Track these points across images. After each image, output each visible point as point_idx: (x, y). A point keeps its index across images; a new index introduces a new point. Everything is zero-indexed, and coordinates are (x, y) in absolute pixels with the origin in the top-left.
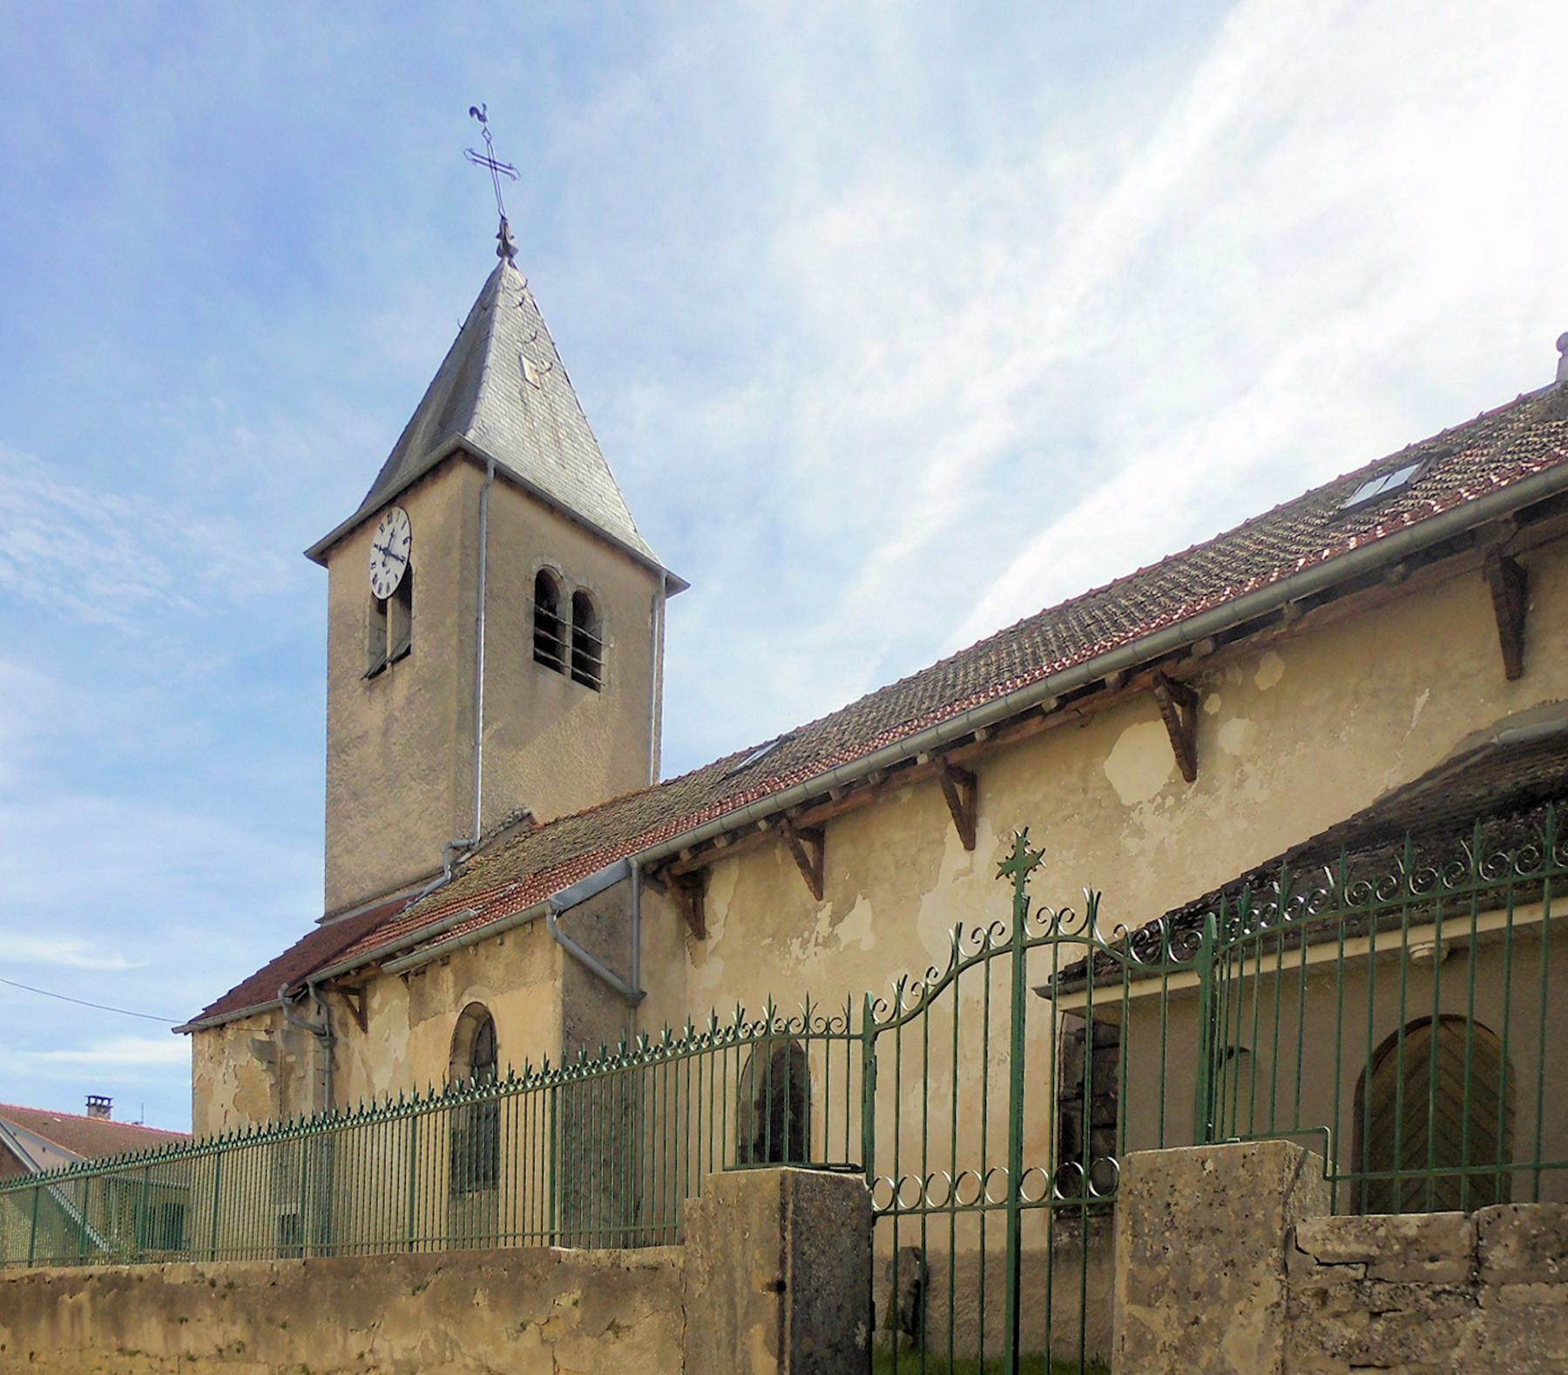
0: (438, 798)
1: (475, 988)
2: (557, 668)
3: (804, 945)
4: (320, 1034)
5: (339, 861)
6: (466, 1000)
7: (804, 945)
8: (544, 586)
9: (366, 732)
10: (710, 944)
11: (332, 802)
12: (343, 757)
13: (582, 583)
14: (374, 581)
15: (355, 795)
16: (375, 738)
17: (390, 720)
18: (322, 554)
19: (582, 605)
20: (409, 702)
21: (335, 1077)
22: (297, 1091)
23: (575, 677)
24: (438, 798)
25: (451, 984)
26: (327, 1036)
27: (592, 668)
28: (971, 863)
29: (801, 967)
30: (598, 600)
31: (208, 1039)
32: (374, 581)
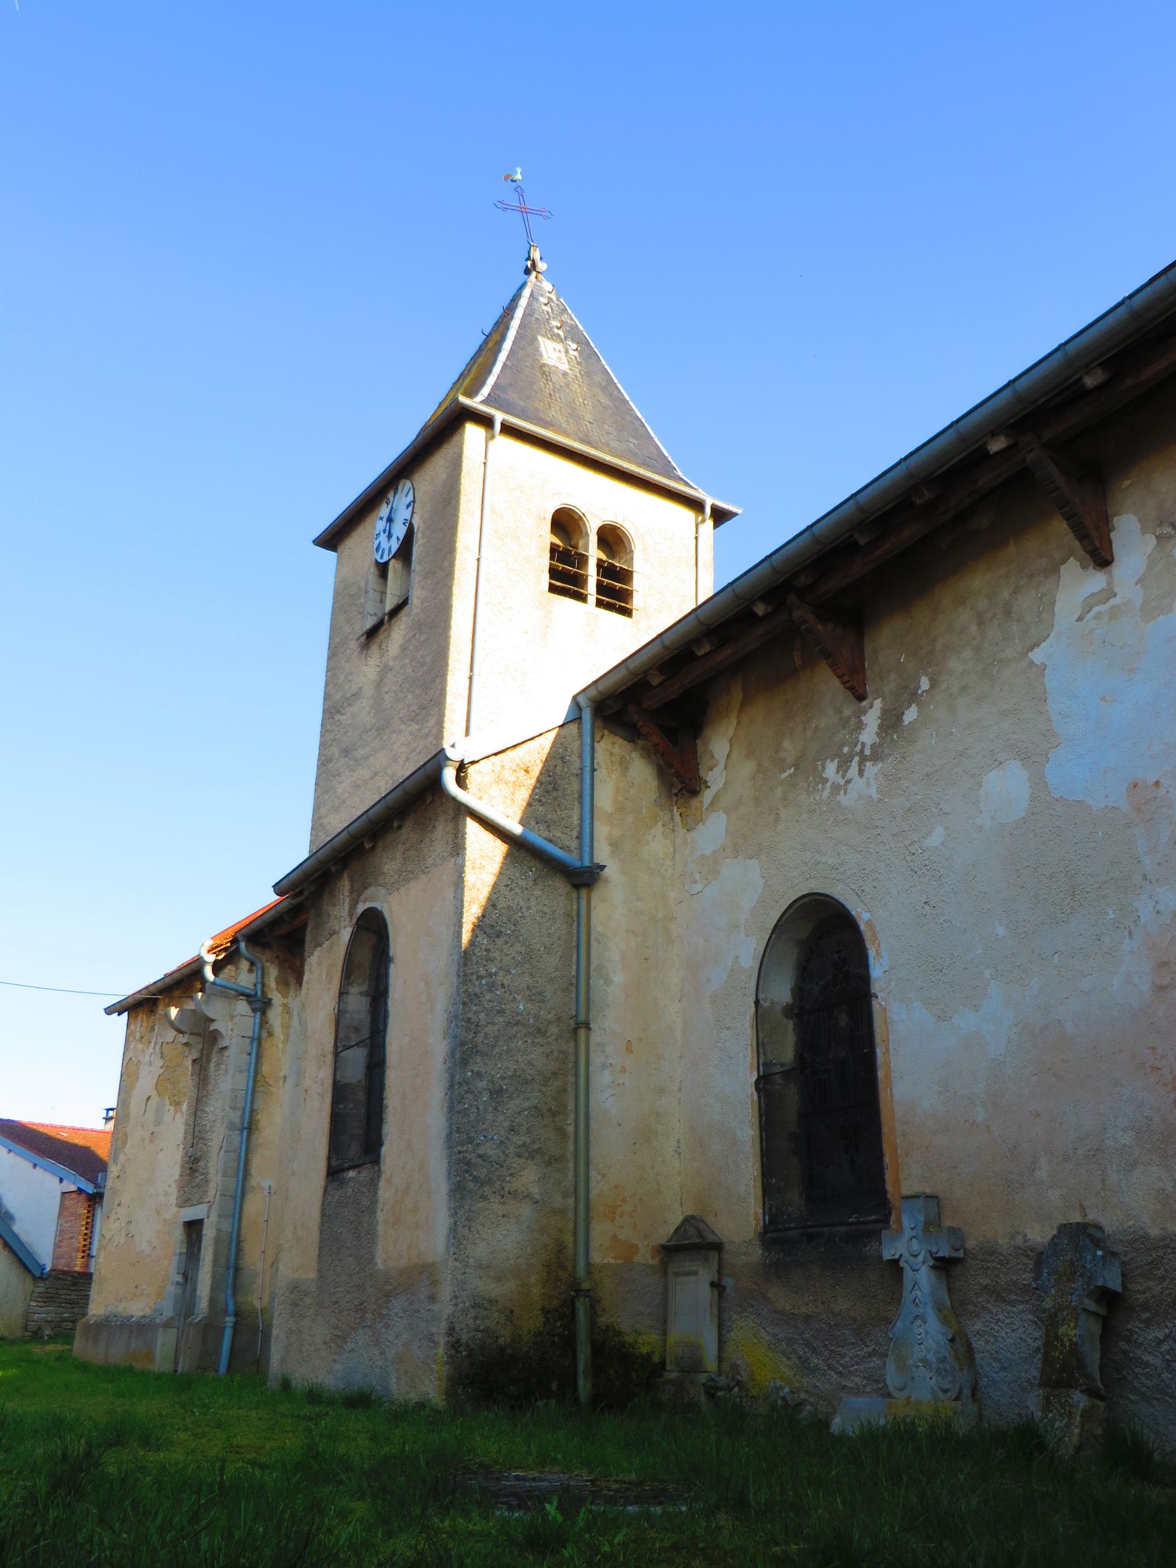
0: (427, 735)
1: (370, 891)
2: (582, 598)
3: (843, 768)
4: (249, 997)
5: (326, 821)
6: (361, 908)
7: (843, 768)
8: (565, 523)
9: (360, 688)
10: (707, 796)
11: (324, 762)
12: (338, 717)
13: (609, 518)
14: (377, 549)
15: (346, 752)
16: (368, 691)
17: (385, 670)
18: (332, 539)
19: (611, 538)
20: (404, 648)
21: (266, 1045)
22: (218, 1065)
23: (599, 603)
24: (427, 735)
25: (347, 893)
26: (260, 1004)
27: (626, 595)
28: (1110, 583)
29: (841, 797)
30: (630, 528)
31: (142, 1016)
32: (377, 549)
